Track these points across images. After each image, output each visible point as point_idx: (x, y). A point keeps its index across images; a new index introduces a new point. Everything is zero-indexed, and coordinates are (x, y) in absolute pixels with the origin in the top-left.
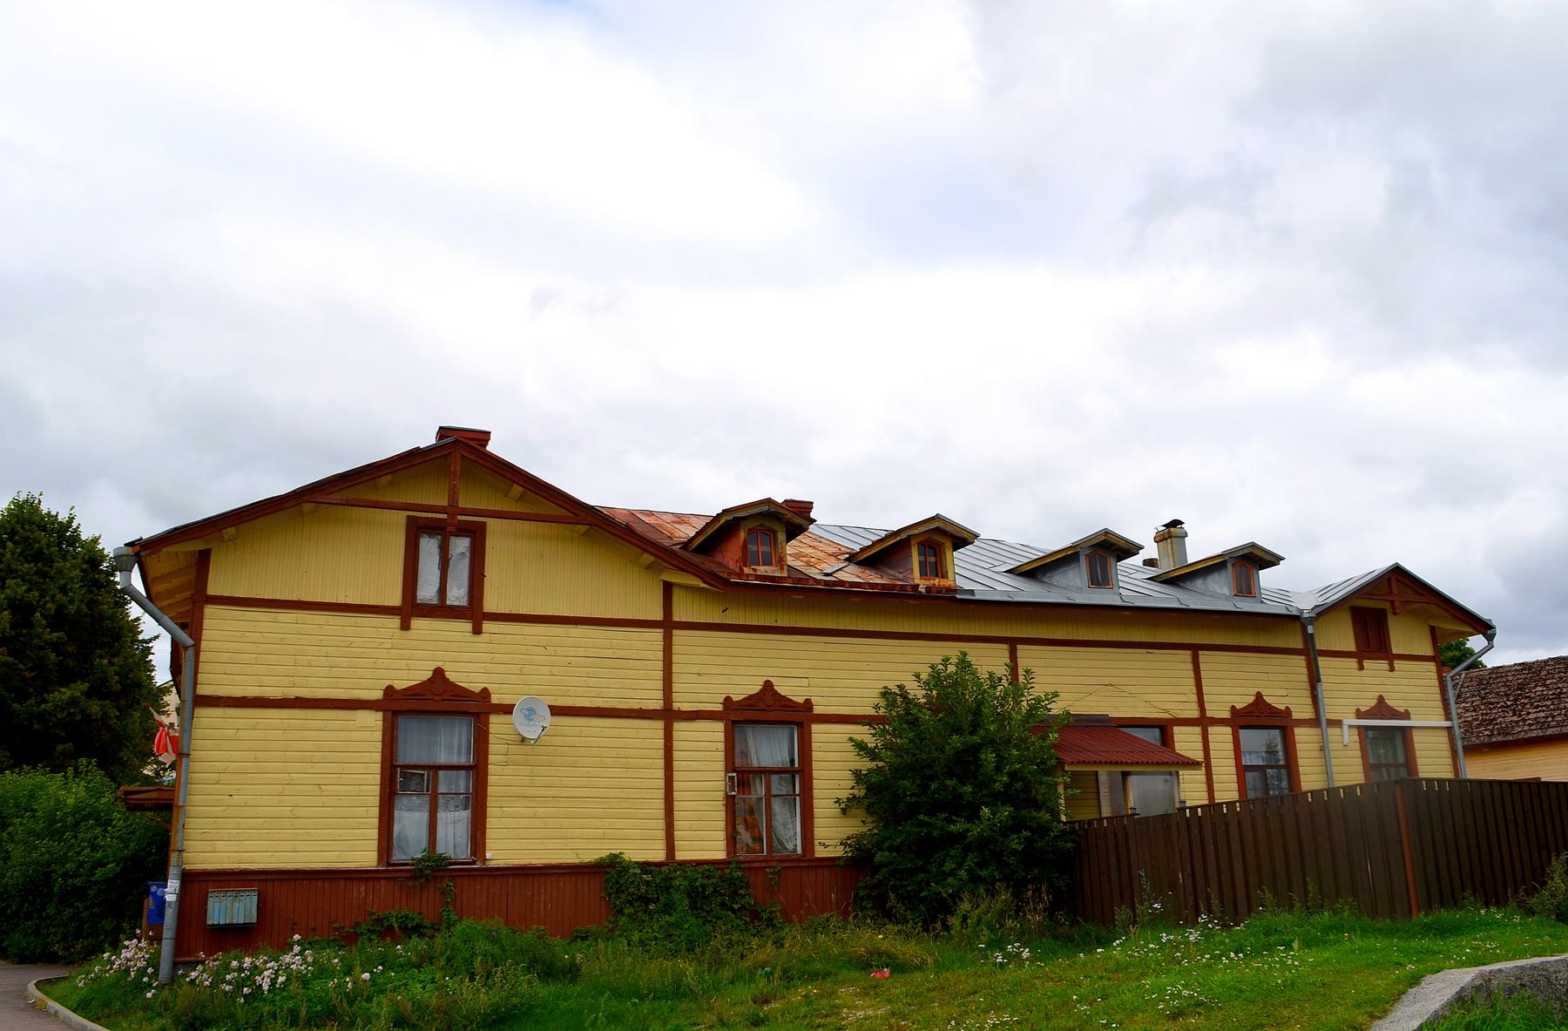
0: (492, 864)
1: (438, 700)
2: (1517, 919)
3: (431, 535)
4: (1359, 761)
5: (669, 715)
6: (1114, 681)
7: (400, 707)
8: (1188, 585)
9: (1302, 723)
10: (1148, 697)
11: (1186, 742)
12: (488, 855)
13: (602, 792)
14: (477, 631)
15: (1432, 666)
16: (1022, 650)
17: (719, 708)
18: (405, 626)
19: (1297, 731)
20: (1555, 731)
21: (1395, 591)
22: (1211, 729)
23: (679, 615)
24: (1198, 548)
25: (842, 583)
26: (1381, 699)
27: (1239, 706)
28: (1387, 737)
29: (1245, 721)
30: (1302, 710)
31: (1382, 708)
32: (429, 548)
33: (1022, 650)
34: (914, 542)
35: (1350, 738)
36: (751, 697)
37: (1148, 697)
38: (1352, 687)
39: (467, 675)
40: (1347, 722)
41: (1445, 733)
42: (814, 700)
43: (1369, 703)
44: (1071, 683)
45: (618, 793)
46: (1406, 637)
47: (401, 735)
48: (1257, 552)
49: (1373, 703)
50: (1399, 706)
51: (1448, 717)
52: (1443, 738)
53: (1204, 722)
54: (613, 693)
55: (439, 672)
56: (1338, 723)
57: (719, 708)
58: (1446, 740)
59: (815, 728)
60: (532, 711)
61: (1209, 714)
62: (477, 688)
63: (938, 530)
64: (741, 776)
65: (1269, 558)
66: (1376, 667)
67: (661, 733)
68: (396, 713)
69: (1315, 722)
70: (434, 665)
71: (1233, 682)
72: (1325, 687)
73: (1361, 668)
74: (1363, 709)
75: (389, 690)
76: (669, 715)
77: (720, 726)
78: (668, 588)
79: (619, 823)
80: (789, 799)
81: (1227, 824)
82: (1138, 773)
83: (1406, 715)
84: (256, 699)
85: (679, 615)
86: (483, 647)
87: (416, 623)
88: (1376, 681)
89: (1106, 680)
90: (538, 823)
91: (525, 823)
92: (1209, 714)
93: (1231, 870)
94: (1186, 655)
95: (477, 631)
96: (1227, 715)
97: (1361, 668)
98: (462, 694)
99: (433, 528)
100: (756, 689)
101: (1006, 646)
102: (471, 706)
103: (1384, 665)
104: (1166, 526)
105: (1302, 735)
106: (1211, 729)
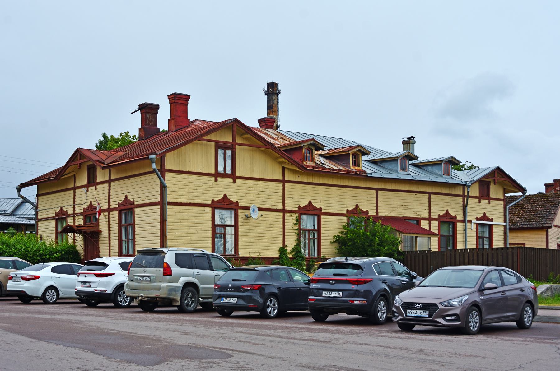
0: (240, 256)
1: (224, 204)
4: (475, 235)
5: (284, 211)
6: (405, 204)
7: (215, 205)
9: (459, 221)
10: (414, 210)
11: (424, 225)
12: (239, 253)
13: (267, 235)
15: (502, 203)
16: (432, 196)
17: (297, 209)
22: (432, 222)
26: (484, 214)
27: (441, 214)
29: (216, 206)
30: (460, 217)
31: (484, 218)
32: (221, 152)
33: (432, 196)
35: (474, 227)
37: (414, 210)
38: (476, 209)
40: (473, 222)
41: (503, 227)
45: (270, 235)
46: (495, 191)
47: (441, 229)
48: (453, 160)
49: (482, 215)
50: (489, 216)
51: (505, 221)
52: (502, 229)
54: (270, 203)
56: (470, 222)
57: (297, 209)
59: (323, 217)
60: (254, 209)
61: (432, 217)
62: (235, 201)
64: (301, 232)
65: (456, 162)
66: (484, 202)
67: (282, 217)
69: (464, 221)
70: (224, 193)
71: (441, 206)
72: (468, 209)
73: (480, 202)
76: (284, 211)
77: (437, 222)
78: (284, 169)
79: (271, 245)
83: (492, 220)
84: (190, 203)
86: (236, 188)
88: (484, 207)
89: (403, 204)
90: (251, 244)
91: (248, 244)
92: (432, 217)
94: (374, 192)
97: (480, 202)
99: (221, 148)
101: (375, 191)
103: (487, 201)
105: (460, 226)
106: (432, 222)
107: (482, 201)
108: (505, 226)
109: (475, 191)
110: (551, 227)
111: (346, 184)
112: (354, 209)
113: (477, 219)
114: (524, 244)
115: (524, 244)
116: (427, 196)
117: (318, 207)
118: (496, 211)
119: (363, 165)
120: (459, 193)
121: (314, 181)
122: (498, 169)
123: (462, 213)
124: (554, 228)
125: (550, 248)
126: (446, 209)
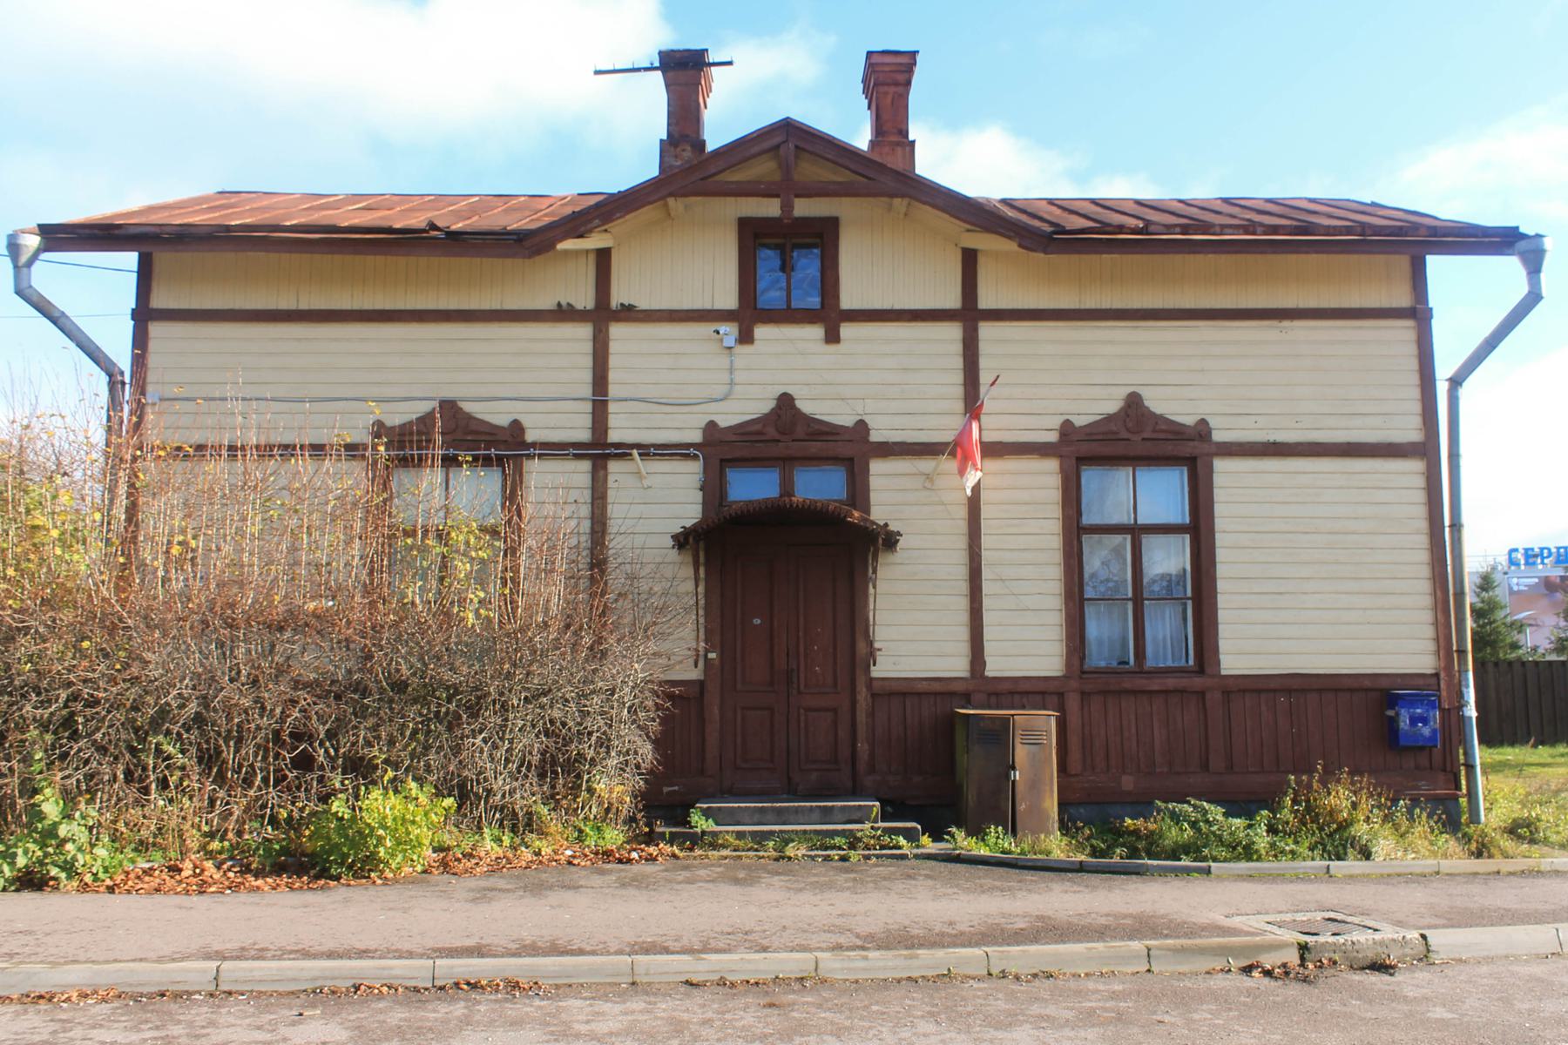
2: (489, 846)
3: (792, 207)
7: (1090, 449)
14: (832, 337)
17: (1053, 437)
18: (746, 337)
23: (987, 299)
36: (1109, 418)
39: (1173, 404)
42: (1213, 423)
68: (726, 462)
75: (1067, 429)
78: (970, 259)
85: (987, 299)
87: (761, 331)
95: (832, 337)
98: (822, 432)
100: (1113, 407)
102: (844, 450)
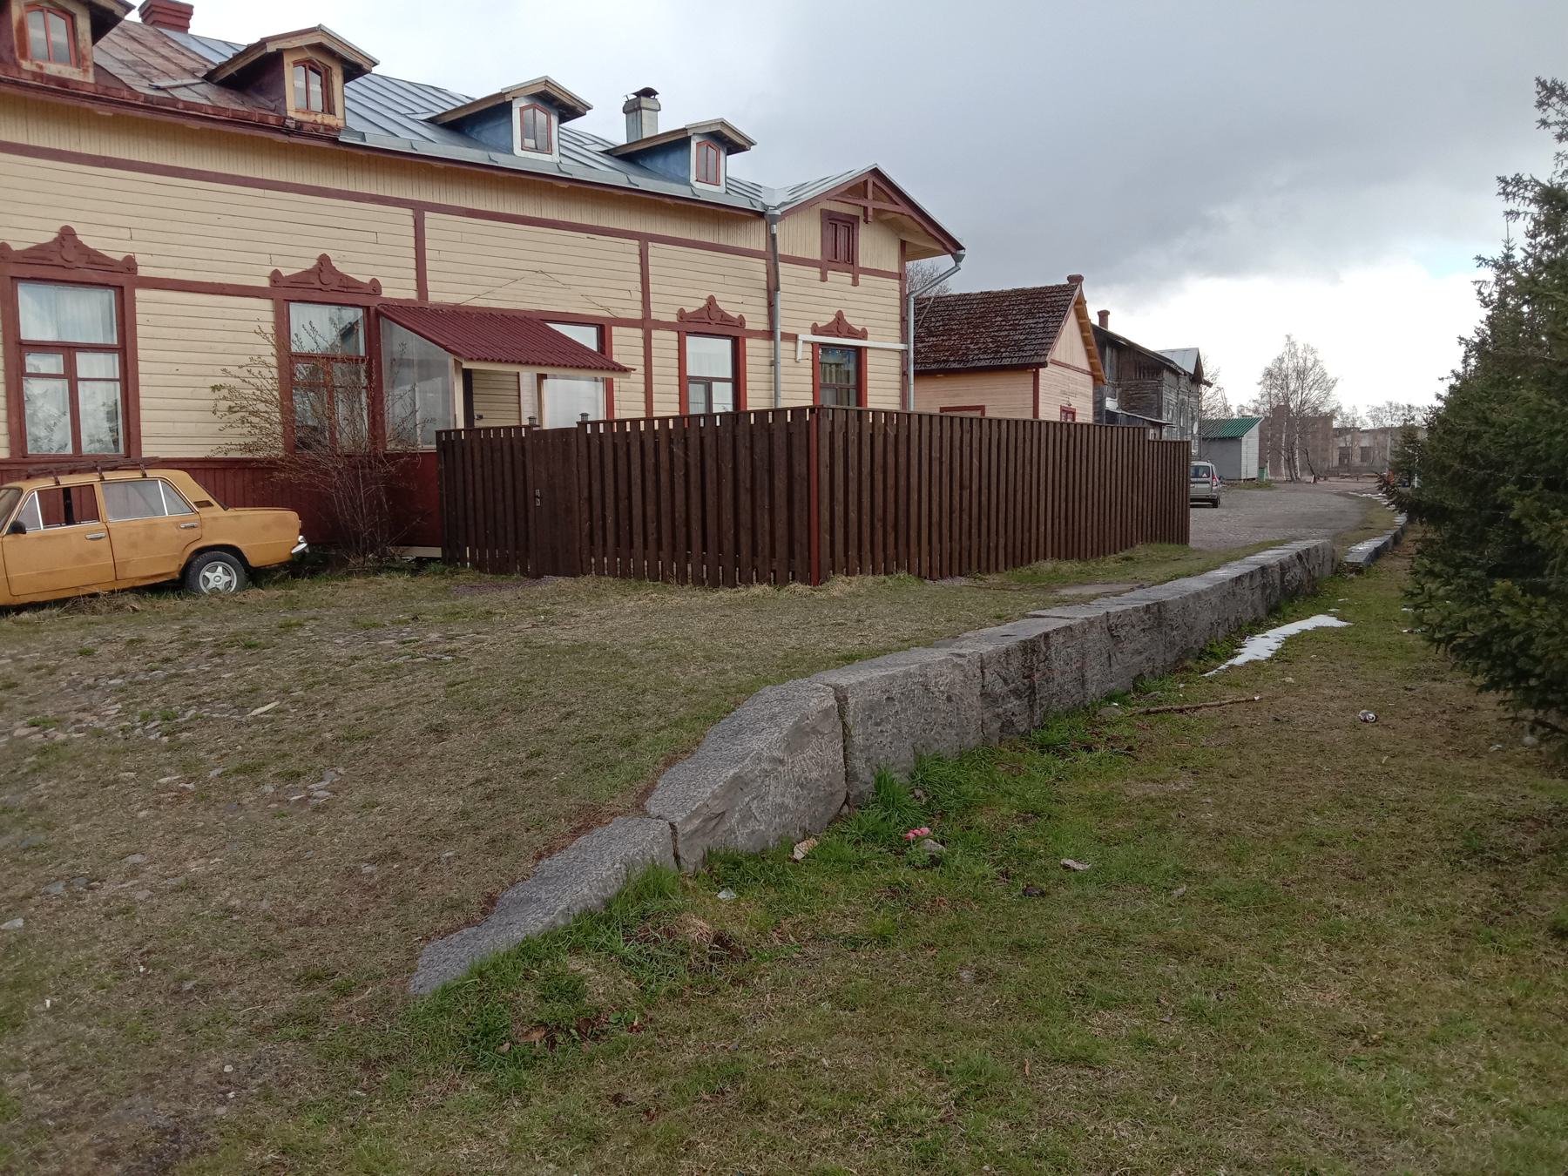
6: (545, 267)
7: (287, 291)
8: (648, 164)
9: (755, 334)
17: (265, 283)
19: (749, 342)
20: (987, 363)
21: (870, 196)
22: (655, 334)
24: (667, 121)
25: (175, 100)
26: (839, 316)
27: (688, 310)
28: (842, 362)
30: (756, 320)
31: (839, 325)
33: (654, 249)
34: (288, 60)
35: (804, 353)
36: (41, 248)
37: (589, 291)
38: (811, 300)
41: (897, 356)
42: (139, 259)
43: (826, 319)
44: (482, 262)
46: (874, 247)
48: (726, 132)
49: (831, 318)
50: (855, 323)
51: (904, 339)
53: (647, 324)
55: (324, 260)
57: (265, 283)
58: (898, 363)
61: (654, 316)
63: (319, 48)
66: (840, 279)
69: (770, 334)
70: (319, 253)
73: (824, 279)
74: (820, 325)
75: (682, 314)
80: (352, 390)
81: (628, 445)
82: (555, 377)
83: (863, 335)
88: (837, 294)
89: (537, 266)
92: (654, 316)
93: (629, 497)
96: (674, 319)
97: (824, 279)
100: (48, 237)
103: (848, 278)
104: (638, 94)
107: (831, 275)
108: (904, 353)
109: (803, 238)
110: (1044, 365)
111: (267, 176)
112: (701, 310)
113: (816, 330)
114: (982, 408)
115: (982, 408)
116: (634, 245)
117: (735, 315)
118: (878, 308)
119: (348, 103)
120: (754, 246)
121: (35, 141)
122: (876, 172)
123: (765, 311)
124: (1050, 368)
125: (1042, 416)
126: (706, 295)
